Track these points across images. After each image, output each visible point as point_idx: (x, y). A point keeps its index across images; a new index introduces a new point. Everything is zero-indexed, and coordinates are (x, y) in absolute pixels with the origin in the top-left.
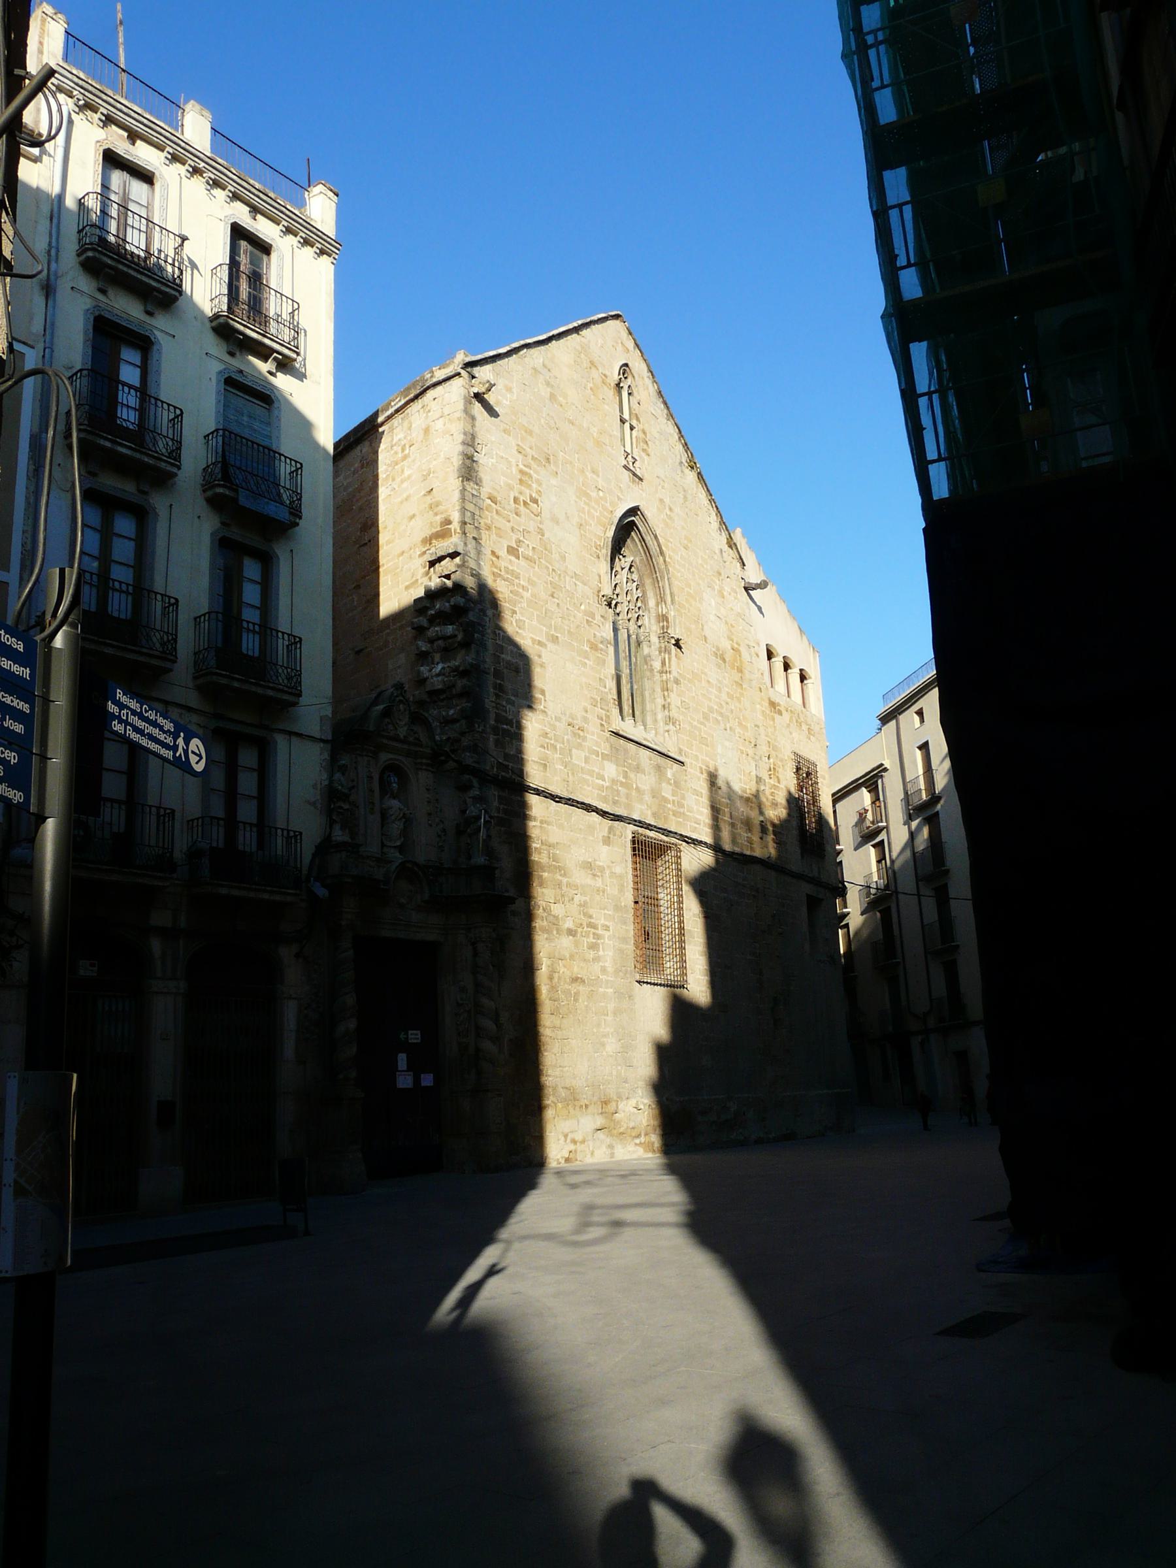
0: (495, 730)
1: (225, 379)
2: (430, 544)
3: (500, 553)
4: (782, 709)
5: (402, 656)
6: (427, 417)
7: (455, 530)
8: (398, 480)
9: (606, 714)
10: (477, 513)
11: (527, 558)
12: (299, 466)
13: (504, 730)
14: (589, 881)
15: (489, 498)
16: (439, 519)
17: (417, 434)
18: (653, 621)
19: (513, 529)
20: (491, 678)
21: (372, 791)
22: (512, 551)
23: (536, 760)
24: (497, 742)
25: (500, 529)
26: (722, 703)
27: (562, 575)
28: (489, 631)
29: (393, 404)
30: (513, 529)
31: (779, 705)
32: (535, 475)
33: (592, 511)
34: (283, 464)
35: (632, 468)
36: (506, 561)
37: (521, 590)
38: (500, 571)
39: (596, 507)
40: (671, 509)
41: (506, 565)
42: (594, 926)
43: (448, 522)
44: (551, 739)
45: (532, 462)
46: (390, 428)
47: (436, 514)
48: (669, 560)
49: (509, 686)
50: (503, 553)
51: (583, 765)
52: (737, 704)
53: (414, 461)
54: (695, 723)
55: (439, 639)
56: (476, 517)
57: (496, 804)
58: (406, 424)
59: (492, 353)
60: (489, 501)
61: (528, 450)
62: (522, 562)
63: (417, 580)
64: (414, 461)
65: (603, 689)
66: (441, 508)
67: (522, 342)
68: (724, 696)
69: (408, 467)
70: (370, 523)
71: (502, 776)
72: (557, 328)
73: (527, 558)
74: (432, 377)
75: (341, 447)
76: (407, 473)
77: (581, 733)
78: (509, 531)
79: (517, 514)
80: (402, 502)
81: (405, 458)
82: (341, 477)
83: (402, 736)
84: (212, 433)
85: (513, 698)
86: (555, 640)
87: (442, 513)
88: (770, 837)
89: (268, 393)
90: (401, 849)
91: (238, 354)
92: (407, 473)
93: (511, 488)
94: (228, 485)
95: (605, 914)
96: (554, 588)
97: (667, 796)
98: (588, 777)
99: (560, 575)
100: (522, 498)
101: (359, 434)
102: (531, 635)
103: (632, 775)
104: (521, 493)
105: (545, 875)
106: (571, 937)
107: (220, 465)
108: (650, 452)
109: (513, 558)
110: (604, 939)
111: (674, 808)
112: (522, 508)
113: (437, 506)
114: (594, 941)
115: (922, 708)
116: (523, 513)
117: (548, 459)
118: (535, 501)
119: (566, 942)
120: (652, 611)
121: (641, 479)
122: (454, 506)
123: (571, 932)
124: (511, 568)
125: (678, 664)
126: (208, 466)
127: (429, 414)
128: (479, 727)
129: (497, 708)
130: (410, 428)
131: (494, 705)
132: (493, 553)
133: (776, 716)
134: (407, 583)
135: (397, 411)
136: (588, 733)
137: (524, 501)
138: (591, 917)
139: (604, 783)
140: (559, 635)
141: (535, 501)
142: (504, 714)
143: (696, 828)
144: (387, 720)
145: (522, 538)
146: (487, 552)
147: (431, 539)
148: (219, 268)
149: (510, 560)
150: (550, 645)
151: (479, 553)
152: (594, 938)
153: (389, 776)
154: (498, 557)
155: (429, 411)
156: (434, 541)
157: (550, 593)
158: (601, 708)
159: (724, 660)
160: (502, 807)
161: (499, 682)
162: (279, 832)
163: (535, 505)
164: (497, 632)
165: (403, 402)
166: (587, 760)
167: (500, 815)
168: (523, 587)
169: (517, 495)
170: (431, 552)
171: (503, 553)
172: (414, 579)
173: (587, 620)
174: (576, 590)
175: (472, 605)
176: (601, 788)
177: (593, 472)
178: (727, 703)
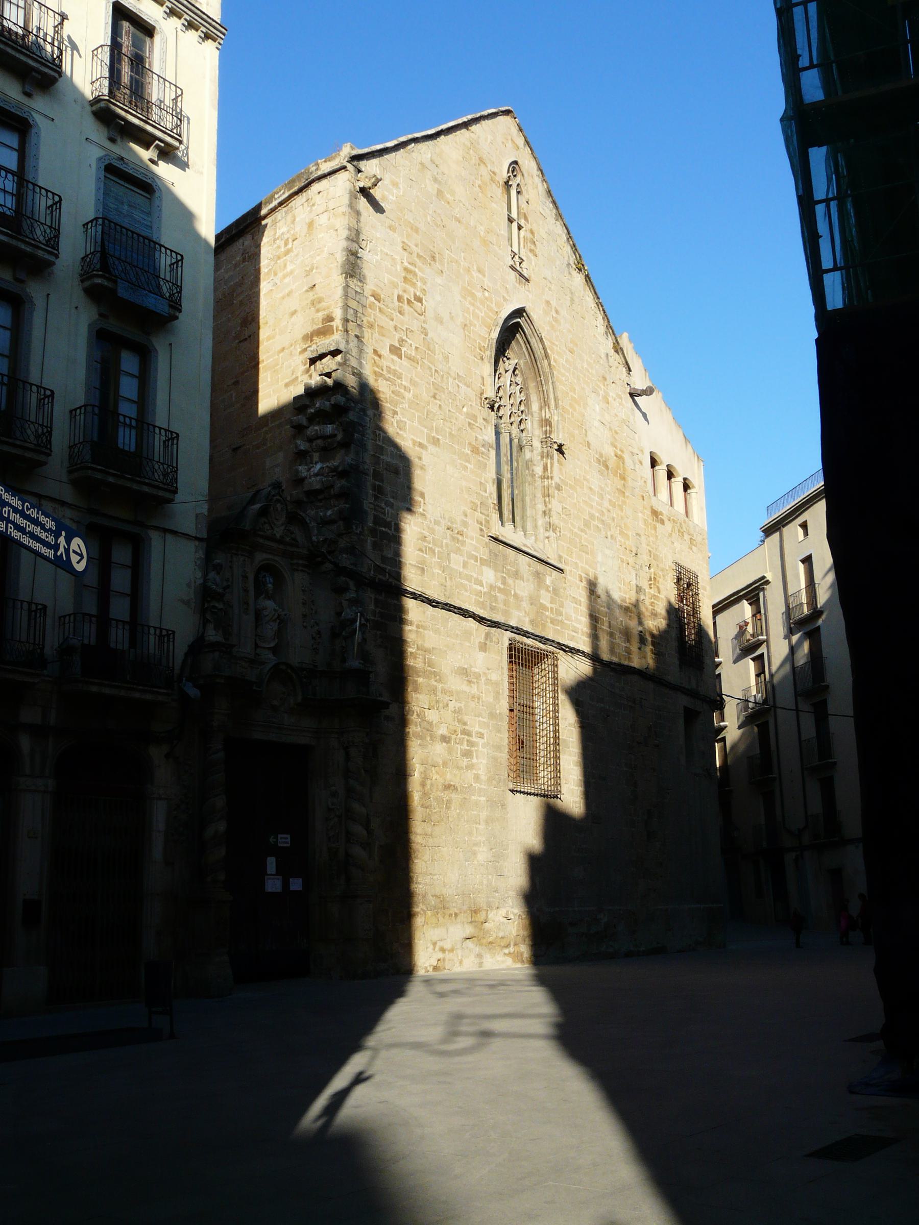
0: (373, 532)
1: (105, 166)
7: (337, 328)
8: (280, 275)
9: (485, 519)
13: (382, 532)
14: (465, 687)
15: (373, 296)
17: (300, 228)
21: (246, 591)
22: (395, 350)
24: (375, 545)
29: (276, 196)
31: (661, 514)
32: (419, 274)
36: (389, 360)
38: (382, 370)
40: (557, 312)
43: (330, 319)
45: (417, 260)
47: (318, 311)
48: (554, 364)
50: (385, 352)
51: (461, 570)
52: (619, 512)
55: (318, 438)
57: (372, 607)
59: (379, 147)
60: (372, 299)
62: (405, 362)
63: (297, 378)
64: (297, 255)
65: (483, 493)
66: (323, 304)
74: (317, 169)
75: (223, 240)
76: (289, 268)
80: (283, 298)
81: (288, 252)
83: (278, 536)
85: (391, 500)
86: (436, 442)
87: (324, 310)
90: (275, 650)
92: (289, 268)
94: (107, 275)
96: (437, 389)
97: (545, 603)
99: (442, 376)
100: (406, 296)
102: (412, 437)
104: (405, 291)
105: (420, 680)
106: (444, 744)
108: (537, 253)
109: (395, 358)
110: (478, 746)
112: (406, 307)
113: (319, 302)
114: (468, 748)
115: (806, 521)
116: (406, 312)
118: (420, 300)
119: (439, 748)
121: (527, 280)
127: (314, 208)
130: (293, 222)
131: (372, 506)
132: (375, 352)
133: (658, 525)
134: (287, 380)
135: (280, 204)
138: (465, 724)
140: (440, 437)
141: (420, 300)
142: (382, 516)
145: (405, 338)
146: (369, 350)
149: (392, 360)
150: (431, 448)
152: (468, 746)
154: (380, 356)
155: (313, 205)
156: (315, 338)
157: (432, 394)
159: (607, 467)
163: (420, 304)
164: (378, 432)
165: (286, 195)
166: (465, 565)
168: (405, 387)
169: (401, 293)
171: (385, 352)
172: (294, 376)
174: (458, 392)
177: (479, 271)
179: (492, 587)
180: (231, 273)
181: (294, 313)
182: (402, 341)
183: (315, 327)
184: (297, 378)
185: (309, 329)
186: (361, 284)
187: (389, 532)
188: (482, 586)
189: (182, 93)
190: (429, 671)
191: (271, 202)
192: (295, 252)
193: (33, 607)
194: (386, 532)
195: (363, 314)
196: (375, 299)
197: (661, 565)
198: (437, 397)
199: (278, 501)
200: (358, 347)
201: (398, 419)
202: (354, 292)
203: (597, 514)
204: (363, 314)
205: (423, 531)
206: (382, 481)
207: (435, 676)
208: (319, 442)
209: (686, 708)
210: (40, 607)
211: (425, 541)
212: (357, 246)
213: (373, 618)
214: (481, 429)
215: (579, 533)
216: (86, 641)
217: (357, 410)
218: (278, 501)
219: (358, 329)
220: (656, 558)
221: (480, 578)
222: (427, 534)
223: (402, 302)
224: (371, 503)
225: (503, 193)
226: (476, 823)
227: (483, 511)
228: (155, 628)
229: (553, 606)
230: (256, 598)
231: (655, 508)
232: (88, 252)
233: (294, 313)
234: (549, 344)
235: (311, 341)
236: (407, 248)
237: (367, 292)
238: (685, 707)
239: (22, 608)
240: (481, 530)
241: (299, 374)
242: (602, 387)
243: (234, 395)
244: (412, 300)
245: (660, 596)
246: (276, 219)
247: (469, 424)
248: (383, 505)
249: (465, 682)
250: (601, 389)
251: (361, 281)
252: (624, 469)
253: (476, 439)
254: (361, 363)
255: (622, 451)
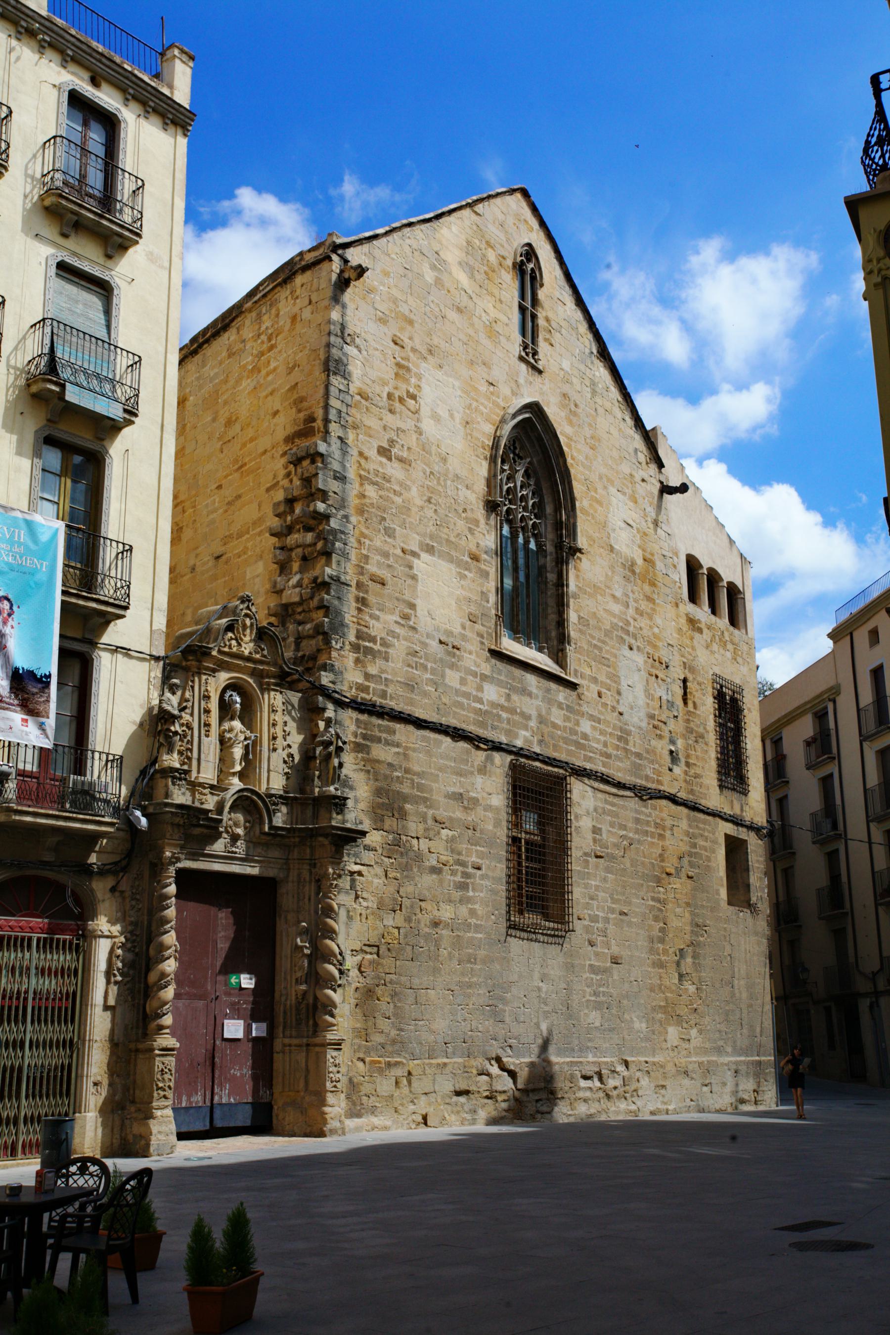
0: (356, 648)
1: (58, 263)
2: (293, 443)
3: (367, 453)
4: (703, 626)
5: (260, 564)
6: (294, 304)
7: (319, 429)
8: (264, 372)
9: (487, 632)
10: (344, 410)
11: (401, 460)
12: (137, 359)
13: (366, 647)
14: (459, 814)
15: (359, 394)
16: (302, 415)
17: (284, 322)
18: (549, 529)
19: (385, 428)
20: (353, 589)
21: (207, 711)
22: (383, 452)
23: (402, 680)
24: (357, 661)
25: (370, 427)
26: (629, 619)
27: (442, 479)
28: (352, 540)
29: (261, 288)
30: (385, 428)
31: (699, 621)
32: (414, 369)
33: (481, 407)
34: (119, 357)
35: (532, 361)
36: (376, 462)
37: (392, 495)
38: (369, 473)
39: (486, 403)
40: (576, 406)
41: (376, 467)
42: (463, 864)
43: (311, 419)
44: (421, 658)
45: (411, 355)
46: (258, 314)
47: (299, 411)
48: (572, 462)
49: (371, 599)
50: (372, 453)
51: (458, 686)
52: (648, 622)
53: (280, 352)
54: (595, 642)
55: (298, 546)
56: (343, 415)
57: (353, 728)
58: (273, 311)
59: (367, 234)
60: (358, 398)
61: (406, 340)
62: (396, 464)
63: (278, 482)
64: (280, 352)
65: (485, 604)
66: (305, 404)
67: (405, 222)
68: (631, 611)
69: (275, 358)
70: (234, 418)
71: (362, 698)
72: (447, 206)
73: (401, 460)
74: (300, 260)
75: (209, 334)
76: (273, 365)
77: (457, 652)
78: (381, 430)
79: (390, 411)
80: (266, 397)
81: (271, 348)
82: (207, 368)
83: (246, 653)
84: (39, 322)
85: (377, 613)
86: (430, 550)
87: (306, 410)
88: (36, 752)
89: (107, 278)
90: (242, 775)
91: (73, 234)
92: (273, 365)
93: (384, 383)
94: (55, 379)
95: (477, 851)
96: (432, 493)
97: (556, 721)
98: (465, 701)
99: (439, 479)
100: (397, 394)
101: (227, 321)
102: (402, 544)
103: (515, 697)
104: (396, 388)
105: (408, 806)
106: (434, 876)
107: (46, 358)
108: (553, 342)
109: (384, 460)
110: (475, 878)
111: (565, 735)
112: (397, 405)
113: (301, 402)
114: (463, 880)
115: (877, 627)
116: (398, 410)
117: (430, 351)
118: (413, 397)
119: (427, 880)
120: (549, 517)
121: (540, 372)
122: (319, 403)
123: (435, 870)
124: (381, 470)
125: (577, 577)
126: (34, 359)
127: (298, 301)
128: (336, 642)
129: (359, 624)
130: (277, 315)
131: (355, 620)
132: (361, 454)
133: (697, 635)
134: (269, 485)
135: (264, 296)
136: (465, 651)
137: (399, 397)
138: (460, 854)
139: (481, 707)
140: (435, 544)
141: (413, 397)
142: (365, 630)
143: (591, 757)
144: (230, 635)
145: (395, 438)
146: (354, 452)
147: (293, 439)
148: (52, 141)
149: (381, 462)
150: (424, 556)
151: (344, 453)
152: (462, 877)
153: (231, 696)
154: (366, 459)
155: (297, 298)
156: (296, 440)
157: (425, 498)
158: (482, 625)
159: (633, 572)
160: (360, 731)
161: (361, 595)
162: (97, 755)
163: (413, 402)
164: (363, 540)
165: (271, 287)
166: (463, 681)
167: (357, 741)
168: (395, 491)
169: (392, 391)
170: (292, 452)
171: (372, 453)
172: (275, 481)
173: (469, 528)
174: (457, 495)
175: (334, 511)
176: (479, 712)
177: (484, 364)
178: (635, 620)
179: (493, 704)
180: (216, 370)
181: (276, 413)
182: (392, 442)
183: (297, 428)
184: (278, 482)
185: (290, 430)
186: (346, 382)
187: (374, 647)
188: (483, 703)
189: (143, 185)
190: (418, 796)
191: (256, 295)
192: (279, 348)
193: (111, 757)
194: (371, 648)
195: (347, 414)
196: (362, 397)
197: (700, 679)
198: (433, 501)
199: (246, 615)
200: (341, 449)
201: (387, 525)
202: (337, 391)
203: (621, 624)
204: (347, 414)
205: (412, 645)
206: (367, 592)
207: (425, 802)
208: (300, 550)
209: (728, 837)
210: (117, 757)
211: (415, 656)
212: (342, 341)
213: (353, 740)
214: (484, 535)
215: (599, 644)
216: (21, 766)
217: (339, 517)
218: (246, 615)
219: (341, 430)
220: (692, 670)
221: (480, 695)
222: (418, 649)
223: (393, 401)
224: (353, 616)
225: (513, 279)
226: (471, 963)
227: (484, 623)
228: (100, 753)
229: (567, 724)
230: (221, 720)
231: (691, 616)
232: (35, 355)
233: (276, 413)
234: (566, 440)
235: (293, 443)
236: (399, 342)
237: (353, 389)
238: (726, 835)
239: (93, 758)
240: (482, 643)
241: (280, 477)
242: (630, 485)
243: (217, 500)
244: (405, 397)
245: (698, 712)
246: (261, 311)
247: (470, 529)
248: (367, 618)
249: (461, 808)
250: (628, 488)
251: (345, 378)
252: (655, 574)
253: (478, 545)
254: (344, 466)
255: (652, 555)
